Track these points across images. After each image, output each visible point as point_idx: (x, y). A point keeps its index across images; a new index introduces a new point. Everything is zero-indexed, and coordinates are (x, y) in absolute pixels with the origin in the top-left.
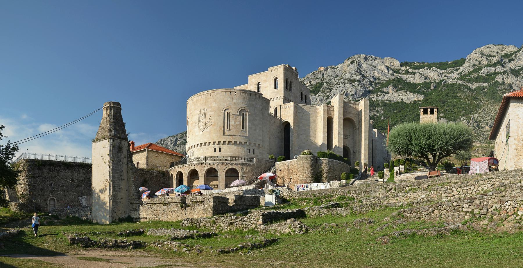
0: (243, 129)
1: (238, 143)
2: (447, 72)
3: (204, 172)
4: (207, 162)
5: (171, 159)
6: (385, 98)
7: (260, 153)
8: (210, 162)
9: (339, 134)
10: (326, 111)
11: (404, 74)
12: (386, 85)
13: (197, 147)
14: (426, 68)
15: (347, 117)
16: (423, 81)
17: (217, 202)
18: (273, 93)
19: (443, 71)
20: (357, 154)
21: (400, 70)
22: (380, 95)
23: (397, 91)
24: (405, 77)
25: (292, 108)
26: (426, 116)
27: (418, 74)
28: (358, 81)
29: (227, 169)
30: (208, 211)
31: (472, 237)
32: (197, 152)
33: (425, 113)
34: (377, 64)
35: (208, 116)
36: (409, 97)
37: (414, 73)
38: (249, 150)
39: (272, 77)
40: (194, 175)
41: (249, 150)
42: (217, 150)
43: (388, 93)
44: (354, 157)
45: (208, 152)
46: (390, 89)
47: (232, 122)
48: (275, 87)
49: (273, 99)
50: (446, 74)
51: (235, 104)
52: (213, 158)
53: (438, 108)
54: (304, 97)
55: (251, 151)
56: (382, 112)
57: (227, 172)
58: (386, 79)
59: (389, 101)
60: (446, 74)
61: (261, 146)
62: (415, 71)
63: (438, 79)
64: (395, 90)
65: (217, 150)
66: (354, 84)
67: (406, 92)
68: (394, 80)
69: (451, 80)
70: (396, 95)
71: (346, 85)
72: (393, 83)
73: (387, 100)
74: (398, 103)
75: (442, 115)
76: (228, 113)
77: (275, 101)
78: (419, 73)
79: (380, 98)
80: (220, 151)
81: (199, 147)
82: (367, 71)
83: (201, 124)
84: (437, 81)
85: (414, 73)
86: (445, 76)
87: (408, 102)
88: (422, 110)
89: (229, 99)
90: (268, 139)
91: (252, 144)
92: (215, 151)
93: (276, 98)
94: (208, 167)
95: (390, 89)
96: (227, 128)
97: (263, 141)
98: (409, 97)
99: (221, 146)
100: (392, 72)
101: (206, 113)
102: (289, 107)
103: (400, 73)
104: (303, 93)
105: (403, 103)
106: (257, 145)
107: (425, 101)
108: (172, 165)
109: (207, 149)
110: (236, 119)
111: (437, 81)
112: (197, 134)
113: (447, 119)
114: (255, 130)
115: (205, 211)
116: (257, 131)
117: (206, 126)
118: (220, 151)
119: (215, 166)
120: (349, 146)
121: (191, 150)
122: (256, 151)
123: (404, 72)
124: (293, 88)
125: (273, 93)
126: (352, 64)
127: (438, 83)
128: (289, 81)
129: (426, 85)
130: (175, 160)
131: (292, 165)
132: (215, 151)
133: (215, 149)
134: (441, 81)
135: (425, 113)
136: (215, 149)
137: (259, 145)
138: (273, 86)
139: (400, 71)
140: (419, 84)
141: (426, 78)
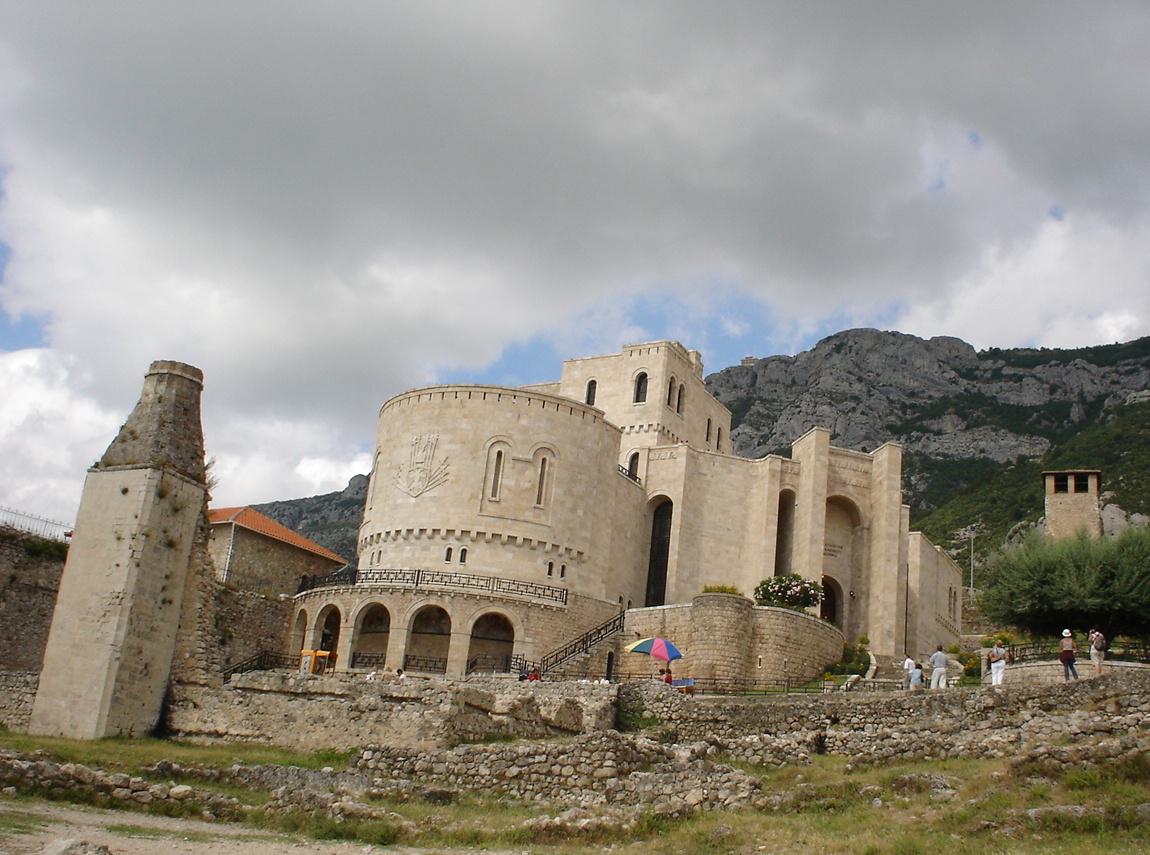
0: (539, 502)
1: (520, 540)
2: (1117, 372)
3: (409, 616)
4: (424, 586)
5: (301, 567)
6: (933, 446)
7: (580, 576)
8: (431, 586)
9: (813, 541)
10: (778, 475)
11: (988, 381)
12: (937, 410)
13: (368, 656)
14: (1053, 362)
15: (837, 493)
16: (1047, 398)
17: (462, 705)
18: (630, 412)
19: (1108, 369)
20: (862, 602)
21: (977, 368)
22: (919, 439)
23: (968, 428)
24: (991, 389)
25: (682, 460)
26: (1062, 496)
27: (1032, 381)
28: (856, 399)
29: (478, 615)
30: (431, 728)
31: (233, 805)
32: (391, 555)
33: (1061, 487)
34: (910, 355)
35: (440, 455)
36: (1003, 447)
37: (1018, 379)
38: (551, 565)
39: (630, 370)
40: (375, 620)
41: (551, 565)
42: (456, 555)
43: (939, 433)
44: (851, 612)
45: (429, 558)
46: (948, 423)
47: (508, 480)
48: (640, 394)
49: (627, 429)
50: (1115, 376)
51: (525, 431)
52: (442, 576)
53: (1099, 476)
54: (714, 432)
55: (556, 569)
56: (922, 488)
57: (477, 625)
58: (936, 395)
59: (945, 456)
60: (1115, 376)
61: (585, 557)
62: (1020, 371)
63: (1092, 390)
64: (963, 425)
65: (456, 555)
66: (841, 407)
67: (995, 430)
68: (958, 396)
69: (1134, 394)
70: (964, 439)
71: (820, 408)
72: (956, 404)
73: (938, 454)
74: (972, 461)
75: (1108, 495)
76: (500, 454)
77: (633, 435)
78: (1035, 377)
79: (918, 447)
80: (463, 559)
81: (400, 540)
82: (880, 371)
83: (417, 474)
84: (1090, 399)
85: (1018, 379)
86: (1113, 382)
87: (1001, 459)
88: (1050, 483)
89: (509, 415)
90: (609, 541)
91: (562, 550)
92: (448, 558)
93: (637, 428)
94: (419, 603)
95: (948, 423)
96: (494, 495)
97: (593, 544)
98: (1003, 447)
99: (467, 543)
100: (953, 374)
101: (435, 446)
102: (672, 457)
103: (975, 378)
104: (713, 423)
105: (987, 463)
106: (574, 554)
107: (1052, 457)
108: (307, 584)
109: (426, 549)
110: (522, 472)
111: (1090, 399)
112: (399, 501)
113: (1123, 507)
114: (574, 510)
115: (425, 729)
116: (580, 512)
117: (431, 481)
118: (463, 559)
119: (445, 604)
120: (843, 579)
121: (376, 548)
122: (569, 570)
123: (988, 375)
124: (687, 404)
125: (630, 412)
126: (838, 352)
127: (1091, 405)
128: (677, 385)
129: (1057, 410)
130: (313, 570)
131: (677, 619)
132: (448, 558)
133: (450, 550)
134: (1101, 398)
135: (1061, 487)
136: (450, 550)
137: (580, 553)
138: (631, 394)
139: (977, 373)
140: (1034, 408)
141: (1053, 390)
